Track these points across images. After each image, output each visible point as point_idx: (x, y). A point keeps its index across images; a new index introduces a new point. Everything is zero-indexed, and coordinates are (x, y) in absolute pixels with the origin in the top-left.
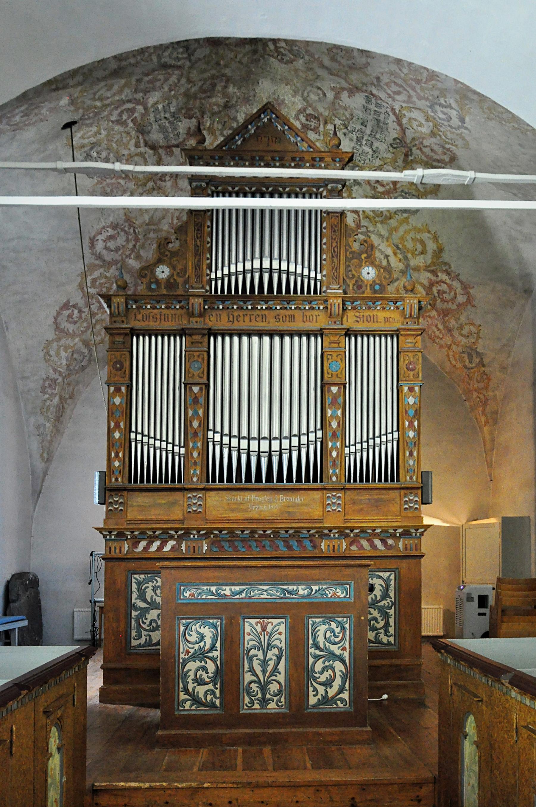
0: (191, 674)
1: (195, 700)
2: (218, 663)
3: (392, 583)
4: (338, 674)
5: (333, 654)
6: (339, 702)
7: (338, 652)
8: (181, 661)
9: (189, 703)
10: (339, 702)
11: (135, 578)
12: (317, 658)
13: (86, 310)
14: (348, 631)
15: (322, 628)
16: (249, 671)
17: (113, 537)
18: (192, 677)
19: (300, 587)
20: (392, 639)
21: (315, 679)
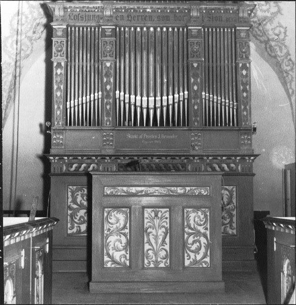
0: (112, 245)
1: (114, 262)
2: (128, 237)
3: (235, 193)
4: (203, 245)
5: (199, 232)
6: (204, 264)
7: (203, 231)
8: (105, 235)
9: (110, 263)
10: (204, 264)
11: (70, 189)
12: (190, 234)
13: (30, 16)
14: (209, 217)
15: (192, 215)
16: (147, 243)
17: (56, 161)
18: (112, 246)
19: (178, 188)
20: (235, 231)
21: (189, 249)
